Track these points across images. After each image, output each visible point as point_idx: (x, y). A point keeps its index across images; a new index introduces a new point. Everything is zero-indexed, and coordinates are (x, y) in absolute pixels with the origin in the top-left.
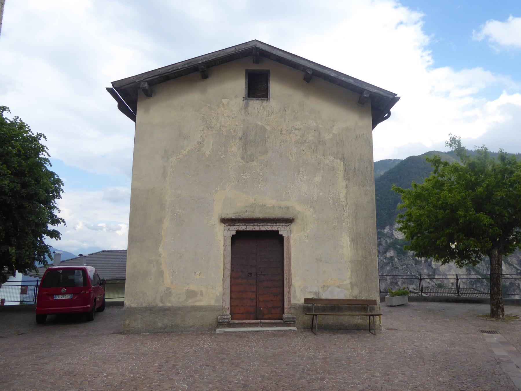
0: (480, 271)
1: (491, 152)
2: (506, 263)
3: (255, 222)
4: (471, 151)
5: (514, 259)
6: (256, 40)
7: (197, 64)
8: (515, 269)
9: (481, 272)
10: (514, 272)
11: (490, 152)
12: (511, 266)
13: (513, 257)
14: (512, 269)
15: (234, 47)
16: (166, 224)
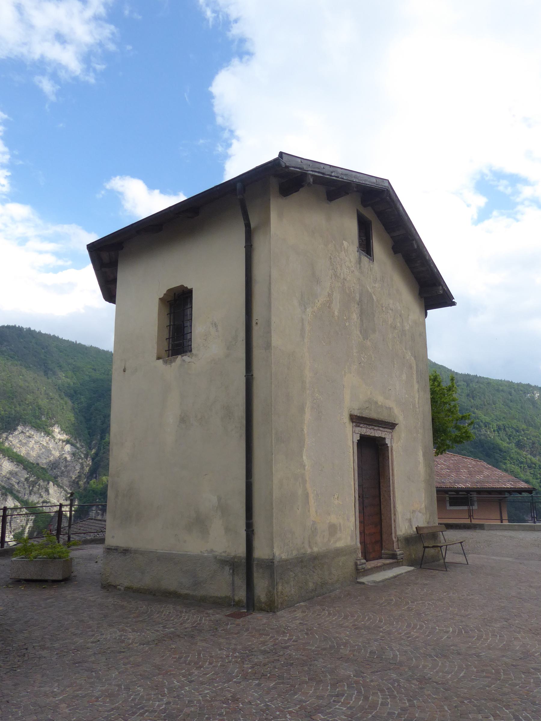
0: (20, 495)
1: (60, 337)
2: (55, 485)
3: (373, 424)
4: (34, 330)
5: (66, 479)
6: (388, 180)
7: (351, 181)
8: (65, 493)
9: (20, 497)
10: (64, 496)
11: (58, 337)
12: (61, 488)
13: (65, 477)
14: (61, 492)
15: (301, 159)
16: (308, 416)
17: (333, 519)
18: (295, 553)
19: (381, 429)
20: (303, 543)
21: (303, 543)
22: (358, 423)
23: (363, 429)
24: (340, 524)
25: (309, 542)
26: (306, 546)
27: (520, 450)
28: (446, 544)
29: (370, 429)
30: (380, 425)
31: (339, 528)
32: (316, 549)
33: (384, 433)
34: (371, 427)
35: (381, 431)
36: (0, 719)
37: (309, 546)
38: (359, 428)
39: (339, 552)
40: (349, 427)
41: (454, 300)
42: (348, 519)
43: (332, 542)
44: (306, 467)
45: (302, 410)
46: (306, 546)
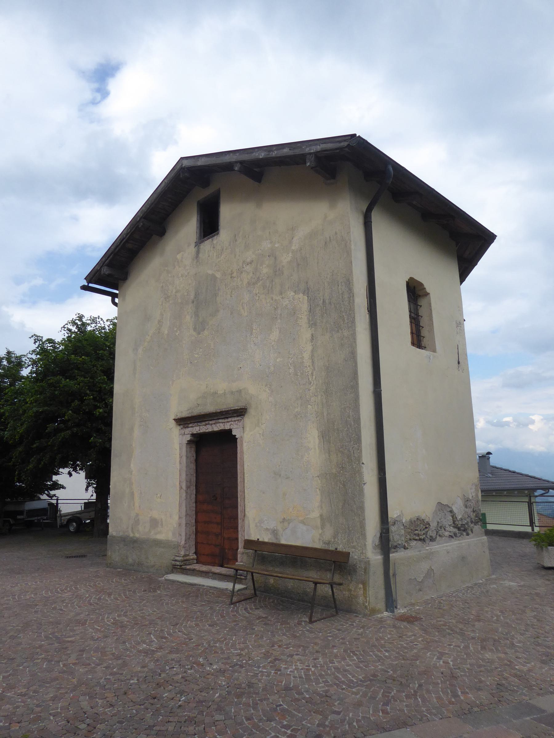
6: (181, 158)
16: (137, 432)
17: (155, 514)
18: (121, 534)
19: (220, 421)
20: (128, 528)
21: (128, 528)
22: (185, 424)
23: (195, 428)
24: (162, 519)
25: (132, 528)
26: (130, 532)
27: (193, 435)
28: (252, 570)
29: (205, 425)
30: (215, 417)
31: (160, 523)
32: (137, 535)
33: (228, 424)
34: (204, 423)
35: (223, 423)
36: (553, 683)
37: (132, 531)
38: (189, 429)
39: (157, 543)
40: (176, 430)
41: (357, 136)
42: (171, 517)
43: (152, 533)
44: (133, 473)
45: (132, 429)
46: (130, 532)
